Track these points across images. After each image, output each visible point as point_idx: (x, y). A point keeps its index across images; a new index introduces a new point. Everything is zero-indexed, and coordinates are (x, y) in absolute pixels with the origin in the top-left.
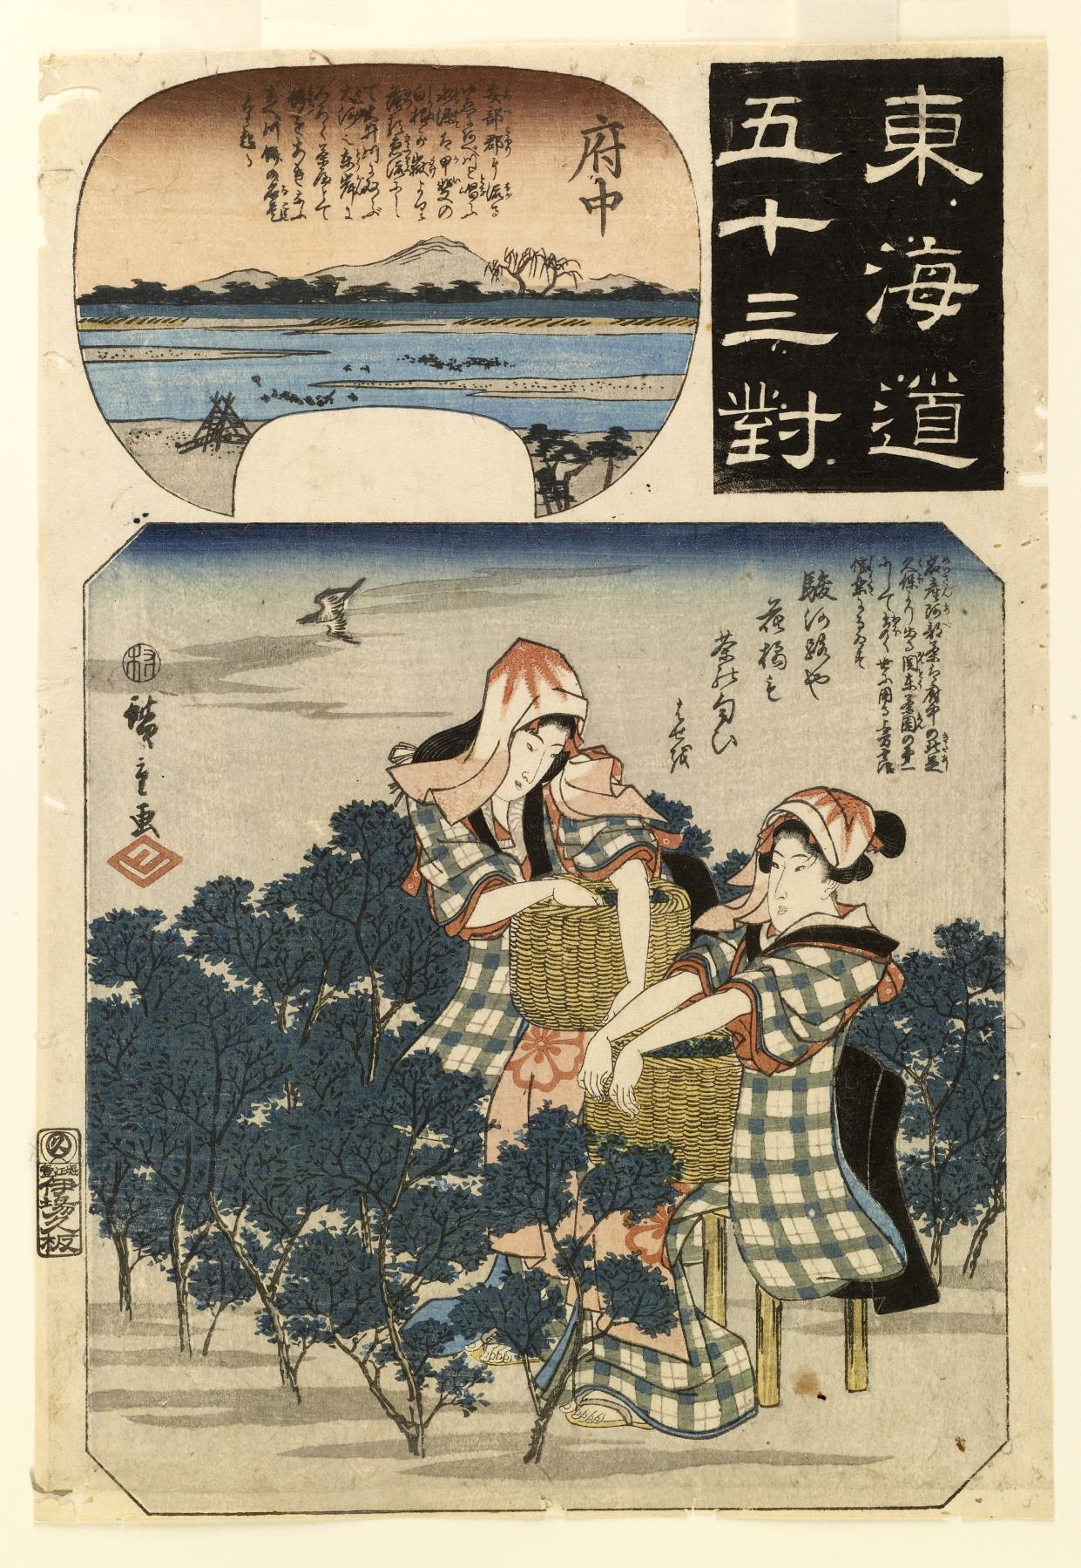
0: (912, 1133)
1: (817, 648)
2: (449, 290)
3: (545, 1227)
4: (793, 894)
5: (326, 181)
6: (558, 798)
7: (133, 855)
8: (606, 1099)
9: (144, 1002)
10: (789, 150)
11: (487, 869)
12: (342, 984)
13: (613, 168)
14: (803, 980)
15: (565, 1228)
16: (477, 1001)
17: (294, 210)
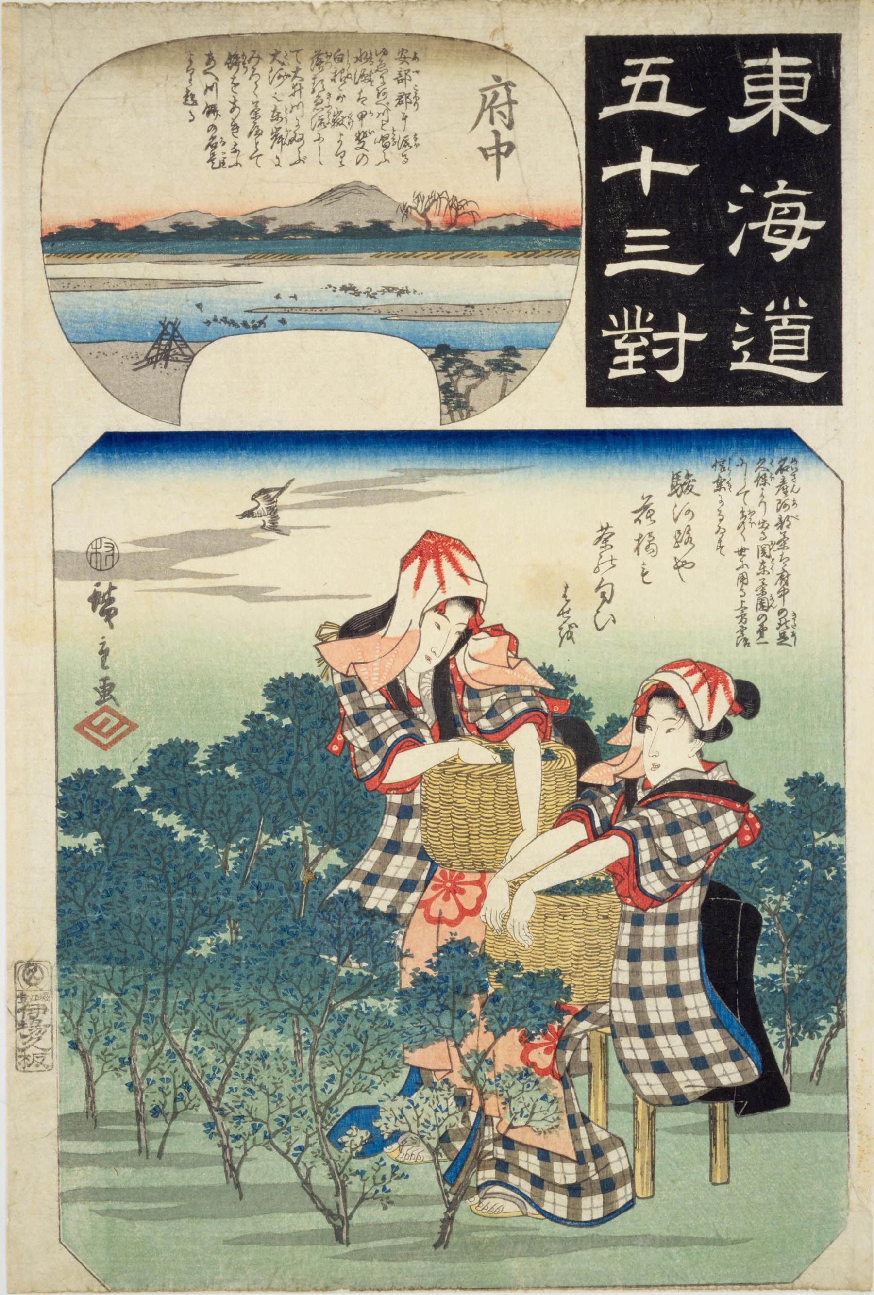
0: (766, 961)
1: (684, 538)
2: (367, 228)
3: (452, 1043)
4: (664, 751)
5: (259, 134)
6: (463, 672)
7: (97, 722)
8: (502, 935)
9: (106, 850)
10: (662, 105)
11: (403, 732)
12: (276, 833)
13: (507, 121)
14: (674, 828)
15: (470, 1043)
16: (393, 847)
17: (231, 159)
